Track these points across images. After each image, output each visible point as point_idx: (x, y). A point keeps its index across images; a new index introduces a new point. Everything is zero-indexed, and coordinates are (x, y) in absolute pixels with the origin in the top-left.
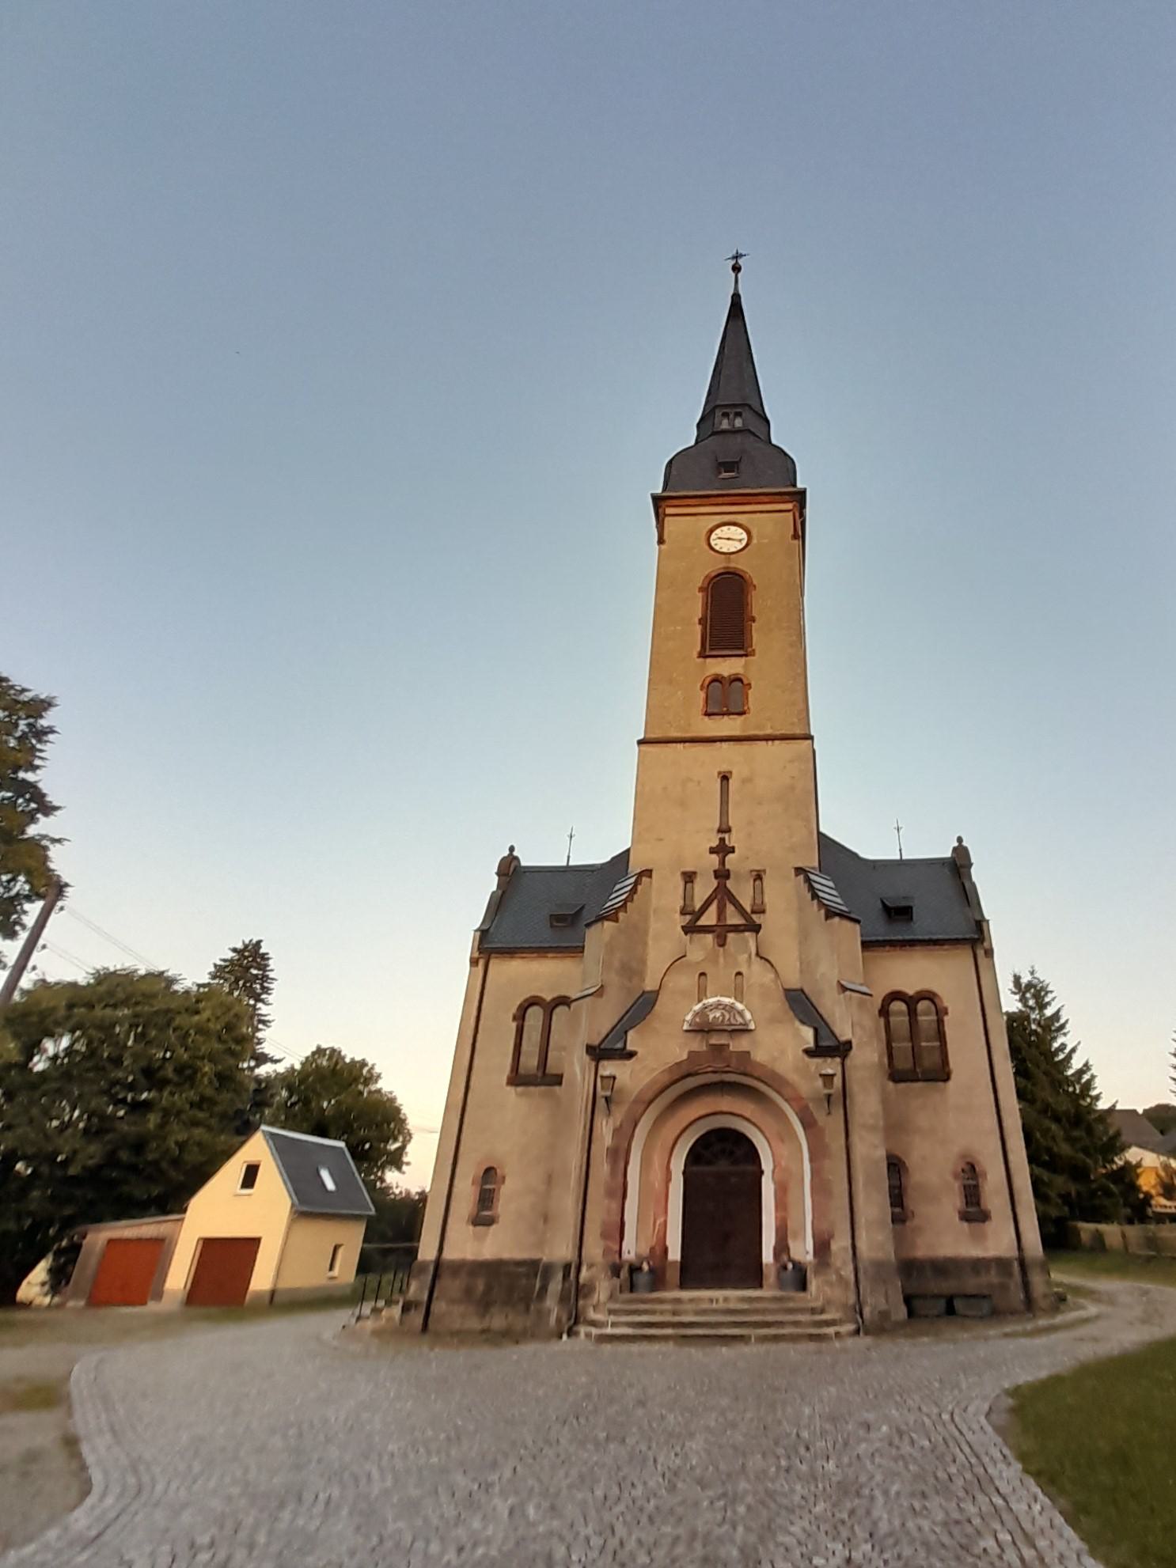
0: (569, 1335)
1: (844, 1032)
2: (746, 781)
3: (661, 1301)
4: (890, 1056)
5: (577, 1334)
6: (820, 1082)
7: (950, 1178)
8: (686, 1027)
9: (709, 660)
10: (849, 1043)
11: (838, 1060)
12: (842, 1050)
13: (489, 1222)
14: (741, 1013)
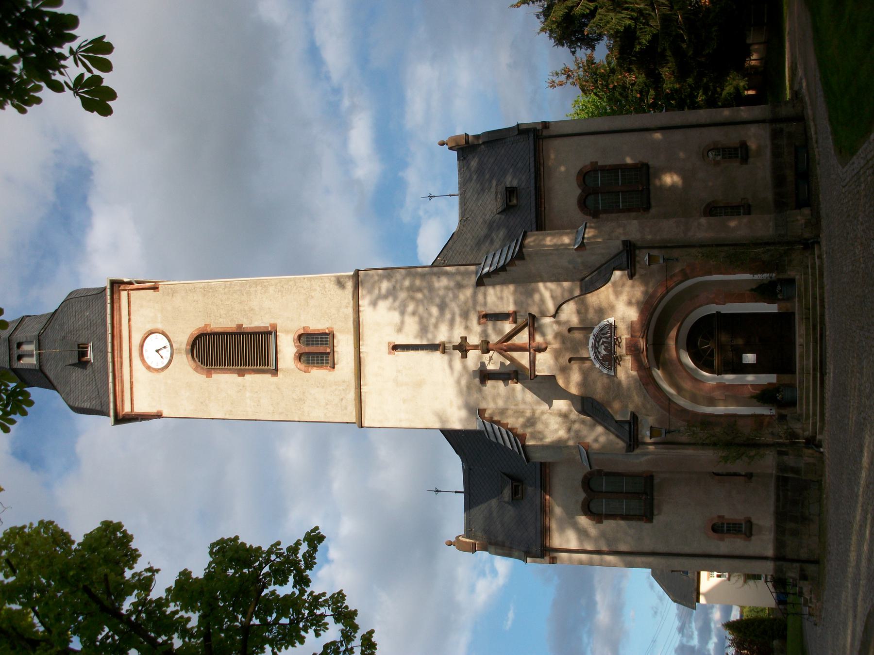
0: (821, 447)
1: (616, 245)
3: (802, 382)
6: (654, 267)
9: (280, 367)
11: (637, 252)
13: (749, 522)
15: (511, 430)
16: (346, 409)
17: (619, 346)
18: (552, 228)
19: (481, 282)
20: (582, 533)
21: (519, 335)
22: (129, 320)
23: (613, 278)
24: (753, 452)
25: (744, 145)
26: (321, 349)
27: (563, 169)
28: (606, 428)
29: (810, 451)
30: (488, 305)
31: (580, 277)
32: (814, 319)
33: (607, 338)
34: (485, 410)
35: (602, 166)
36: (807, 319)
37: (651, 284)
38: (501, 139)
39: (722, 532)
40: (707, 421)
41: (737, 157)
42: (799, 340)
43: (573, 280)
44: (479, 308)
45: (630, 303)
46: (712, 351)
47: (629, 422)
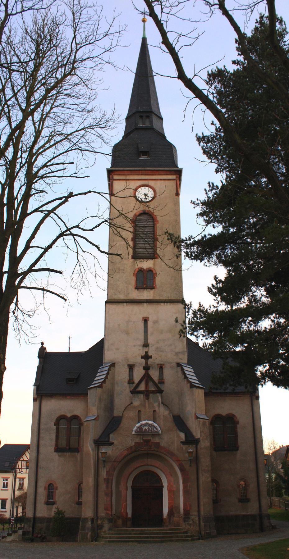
2: (156, 322)
6: (187, 455)
8: (133, 433)
11: (194, 446)
13: (54, 503)
14: (156, 427)
22: (161, 180)
25: (248, 500)
39: (49, 489)
47: (108, 441)
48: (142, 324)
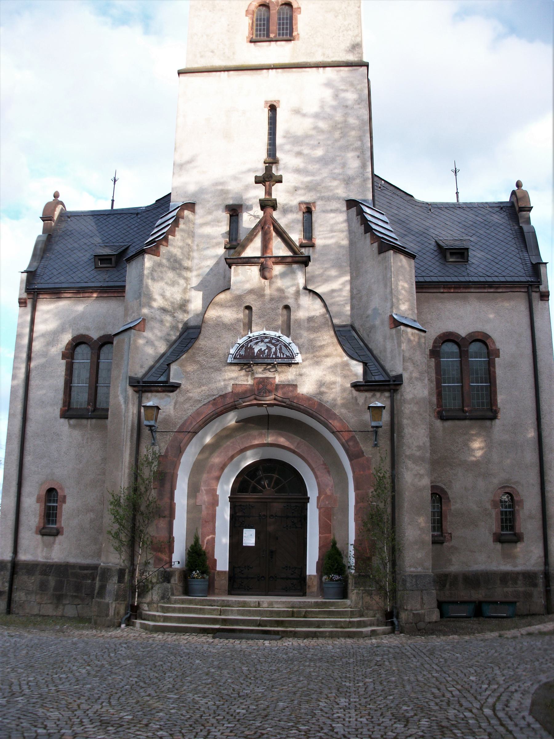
0: (127, 625)
1: (395, 367)
4: (439, 395)
5: (133, 624)
6: (367, 416)
7: (489, 506)
10: (399, 379)
11: (387, 394)
12: (392, 385)
13: (57, 533)
15: (166, 239)
16: (202, 56)
17: (265, 369)
18: (418, 299)
19: (352, 204)
20: (53, 336)
21: (283, 245)
23: (354, 362)
24: (123, 537)
25: (517, 538)
26: (274, 27)
27: (491, 316)
28: (163, 355)
29: (122, 611)
30: (323, 215)
31: (357, 325)
32: (290, 624)
33: (275, 353)
34: (193, 211)
35: (494, 363)
36: (293, 614)
37: (343, 411)
38: (526, 246)
40: (165, 479)
41: (502, 529)
42: (265, 600)
43: (352, 316)
44: (319, 203)
45: (321, 384)
46: (261, 491)
47: (167, 381)
48: (265, 114)
